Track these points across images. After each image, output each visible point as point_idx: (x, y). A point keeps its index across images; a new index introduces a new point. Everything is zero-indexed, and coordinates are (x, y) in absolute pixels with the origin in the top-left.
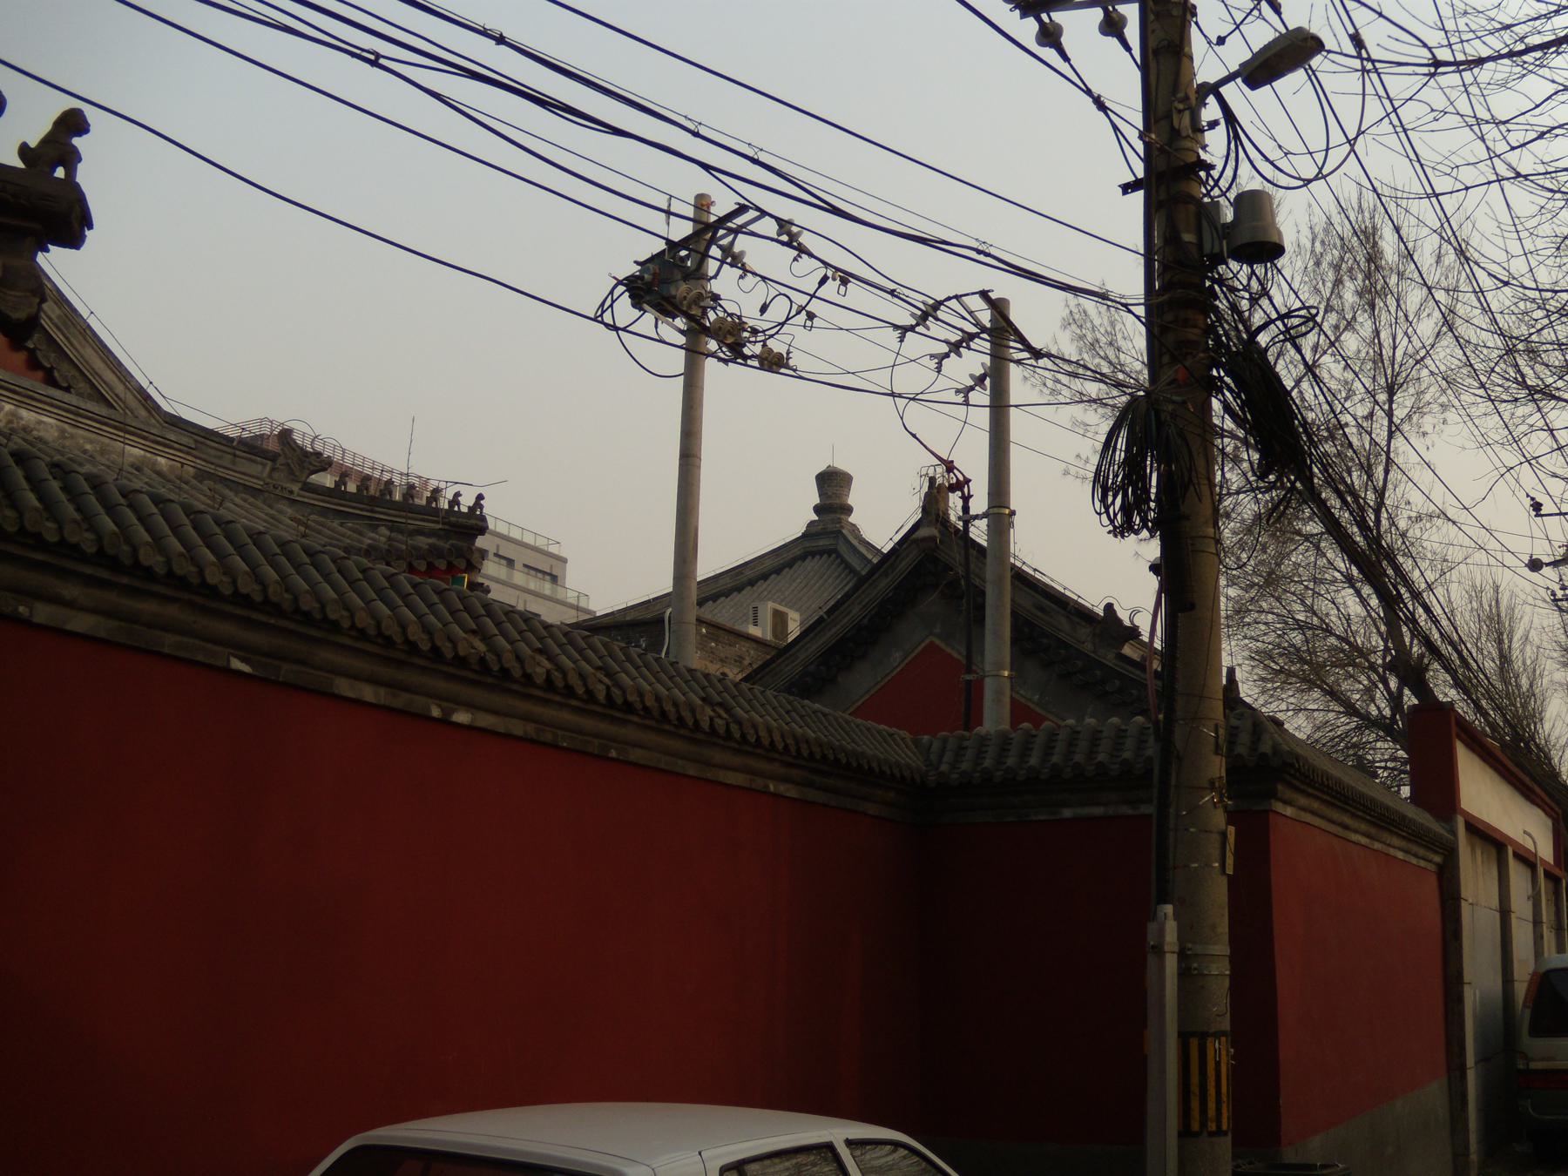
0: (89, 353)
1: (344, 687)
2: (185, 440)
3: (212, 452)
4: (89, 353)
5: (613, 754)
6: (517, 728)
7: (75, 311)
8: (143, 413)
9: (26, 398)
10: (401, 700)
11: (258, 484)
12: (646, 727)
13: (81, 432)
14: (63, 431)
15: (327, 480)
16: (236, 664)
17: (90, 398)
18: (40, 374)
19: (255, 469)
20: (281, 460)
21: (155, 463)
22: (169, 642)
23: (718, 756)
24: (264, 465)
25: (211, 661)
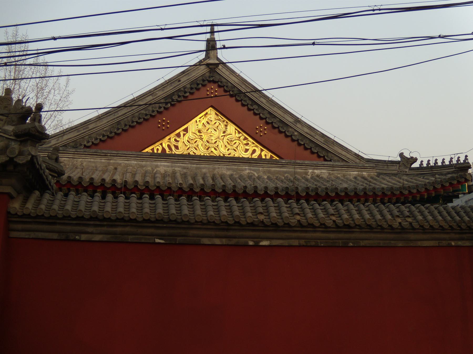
0: (336, 148)
1: (206, 241)
2: (372, 165)
3: (381, 166)
4: (336, 148)
5: (351, 244)
6: (296, 243)
7: (329, 138)
8: (358, 161)
9: (316, 167)
10: (234, 241)
11: (395, 172)
12: (361, 232)
13: (335, 172)
14: (329, 173)
15: (416, 165)
16: (157, 241)
17: (338, 161)
18: (322, 159)
19: (394, 168)
20: (401, 163)
21: (362, 175)
22: (130, 238)
23: (413, 236)
24: (396, 166)
25: (148, 241)
